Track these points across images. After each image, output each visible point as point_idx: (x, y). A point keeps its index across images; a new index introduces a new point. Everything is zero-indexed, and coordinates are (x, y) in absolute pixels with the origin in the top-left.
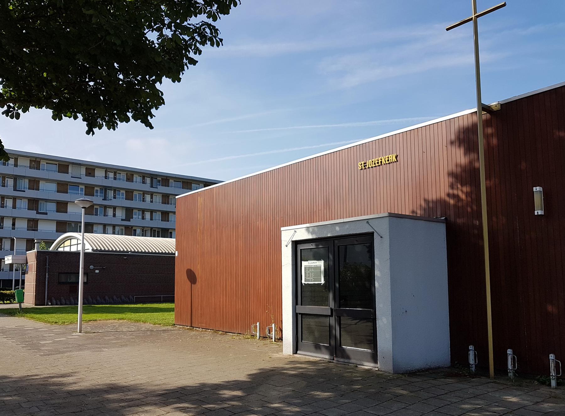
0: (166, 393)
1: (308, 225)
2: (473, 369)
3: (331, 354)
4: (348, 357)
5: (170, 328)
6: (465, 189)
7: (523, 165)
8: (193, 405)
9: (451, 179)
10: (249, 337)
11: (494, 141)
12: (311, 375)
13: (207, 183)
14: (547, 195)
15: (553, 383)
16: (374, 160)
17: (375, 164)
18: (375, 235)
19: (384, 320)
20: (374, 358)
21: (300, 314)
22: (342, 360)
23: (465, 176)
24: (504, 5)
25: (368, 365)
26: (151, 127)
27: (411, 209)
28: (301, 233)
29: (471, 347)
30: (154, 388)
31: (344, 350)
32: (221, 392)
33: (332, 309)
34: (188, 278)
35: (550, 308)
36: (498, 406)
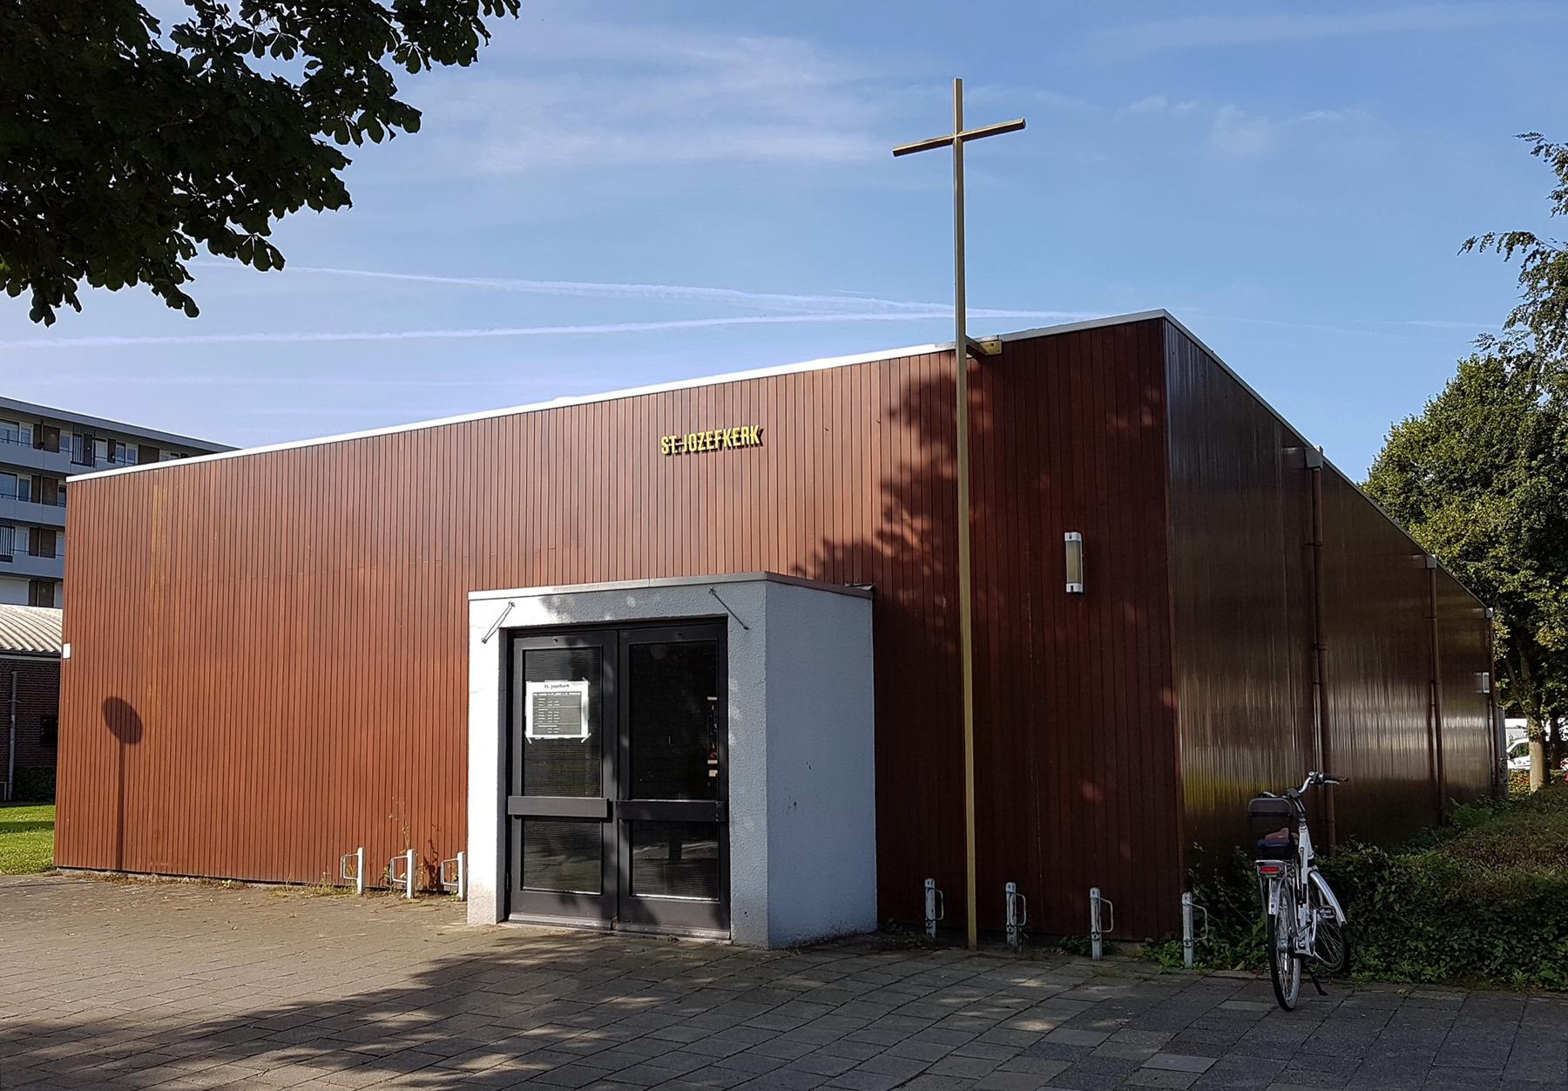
0: (216, 1032)
1: (549, 590)
2: (933, 931)
3: (605, 916)
4: (651, 920)
5: (40, 878)
6: (918, 524)
7: (1045, 481)
8: (319, 1048)
9: (887, 499)
10: (329, 890)
11: (986, 421)
12: (577, 965)
13: (150, 447)
14: (1088, 548)
15: (1096, 948)
16: (702, 435)
17: (705, 444)
18: (731, 622)
19: (749, 824)
20: (721, 916)
21: (517, 817)
22: (635, 927)
23: (920, 494)
24: (1021, 126)
25: (705, 935)
26: (193, 311)
27: (792, 559)
28: (530, 608)
29: (929, 883)
30: (164, 1023)
31: (639, 902)
32: (369, 1017)
33: (610, 804)
34: (109, 723)
35: (1089, 791)
36: (1008, 997)
